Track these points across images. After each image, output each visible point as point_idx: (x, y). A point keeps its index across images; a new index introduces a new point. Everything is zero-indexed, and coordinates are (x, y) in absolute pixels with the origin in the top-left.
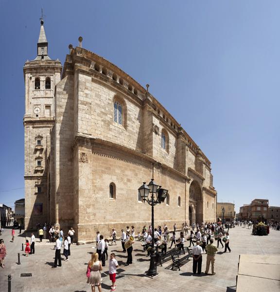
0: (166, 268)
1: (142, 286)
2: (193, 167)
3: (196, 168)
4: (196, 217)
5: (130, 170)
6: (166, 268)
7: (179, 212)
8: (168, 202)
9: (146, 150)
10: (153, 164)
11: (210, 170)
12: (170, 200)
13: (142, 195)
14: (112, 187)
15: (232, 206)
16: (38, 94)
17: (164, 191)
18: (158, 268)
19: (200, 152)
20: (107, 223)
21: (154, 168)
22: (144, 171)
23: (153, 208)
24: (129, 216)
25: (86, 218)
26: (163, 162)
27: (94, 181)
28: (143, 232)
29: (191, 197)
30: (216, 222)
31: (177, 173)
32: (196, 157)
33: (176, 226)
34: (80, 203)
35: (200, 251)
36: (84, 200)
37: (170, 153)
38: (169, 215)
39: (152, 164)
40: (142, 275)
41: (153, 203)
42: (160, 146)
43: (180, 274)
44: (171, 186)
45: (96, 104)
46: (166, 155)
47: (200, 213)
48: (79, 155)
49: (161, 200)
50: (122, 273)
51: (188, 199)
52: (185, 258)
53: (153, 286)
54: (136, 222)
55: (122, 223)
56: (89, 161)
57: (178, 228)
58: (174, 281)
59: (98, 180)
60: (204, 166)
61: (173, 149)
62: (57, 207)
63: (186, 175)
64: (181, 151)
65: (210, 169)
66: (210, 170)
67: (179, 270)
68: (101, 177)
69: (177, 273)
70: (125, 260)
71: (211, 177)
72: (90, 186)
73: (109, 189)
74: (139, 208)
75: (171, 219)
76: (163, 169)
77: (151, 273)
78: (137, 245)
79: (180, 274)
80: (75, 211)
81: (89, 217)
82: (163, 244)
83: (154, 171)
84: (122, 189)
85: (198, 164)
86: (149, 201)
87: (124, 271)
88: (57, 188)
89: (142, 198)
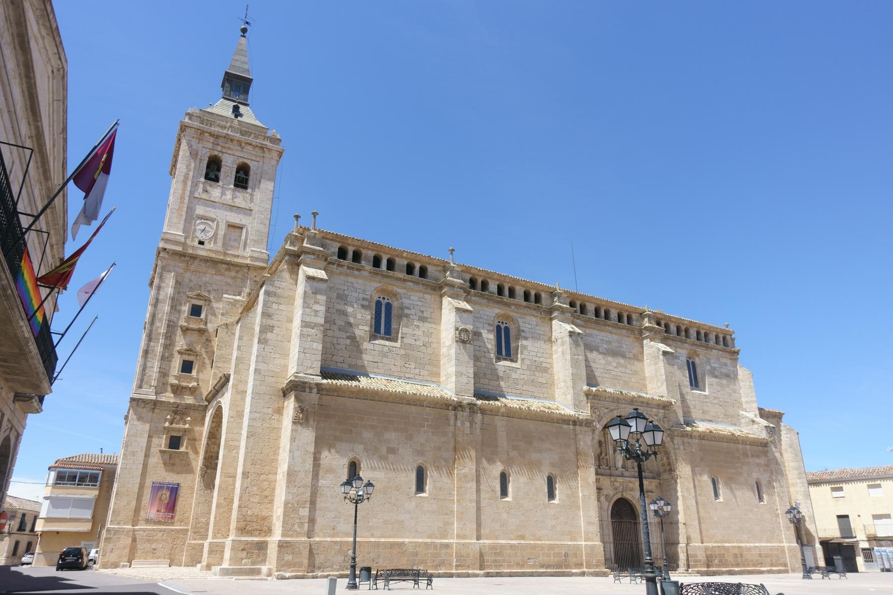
16: (215, 192)
25: (296, 527)
45: (337, 310)
54: (407, 540)
75: (522, 537)
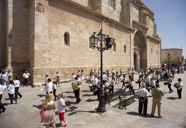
0: (113, 107)
1: (93, 121)
2: (137, 20)
3: (139, 20)
4: (141, 63)
5: (83, 23)
6: (113, 107)
7: (125, 58)
8: (115, 50)
9: (96, 8)
10: (102, 18)
11: (153, 20)
12: (117, 48)
13: (93, 42)
14: (67, 37)
15: (179, 52)
17: (112, 40)
18: (107, 106)
19: (143, 6)
20: (62, 67)
21: (103, 22)
22: (94, 24)
23: (101, 54)
24: (81, 61)
25: (42, 62)
26: (110, 17)
27: (50, 29)
28: (91, 75)
29: (135, 45)
30: (160, 67)
31: (122, 25)
32: (139, 11)
33: (122, 70)
34: (36, 48)
35: (146, 94)
36: (40, 45)
37: (117, 10)
38: (116, 61)
39: (101, 18)
40: (92, 112)
41: (102, 50)
42: (108, 5)
43: (127, 113)
44: (117, 36)
46: (113, 11)
47: (144, 59)
48: (36, 4)
49: (108, 46)
50: (74, 110)
51: (133, 47)
52: (131, 98)
53: (102, 121)
54: (87, 66)
55: (75, 67)
56: (46, 12)
57: (123, 72)
58: (121, 118)
59: (54, 29)
60: (147, 17)
61: (119, 7)
62: (10, 50)
63: (131, 27)
64: (126, 8)
65: (154, 19)
66: (153, 20)
67: (126, 109)
68: (56, 26)
69: (124, 111)
70: (75, 100)
71: (155, 26)
72: (46, 33)
73: (64, 38)
74: (90, 54)
75: (118, 64)
76: (110, 22)
77: (100, 110)
78: (84, 86)
79: (127, 113)
80: (31, 55)
81: (44, 61)
82: (110, 85)
83: (103, 24)
84: (75, 38)
85: (142, 17)
86: (98, 48)
87: (77, 108)
88: (9, 30)
89: (92, 46)
